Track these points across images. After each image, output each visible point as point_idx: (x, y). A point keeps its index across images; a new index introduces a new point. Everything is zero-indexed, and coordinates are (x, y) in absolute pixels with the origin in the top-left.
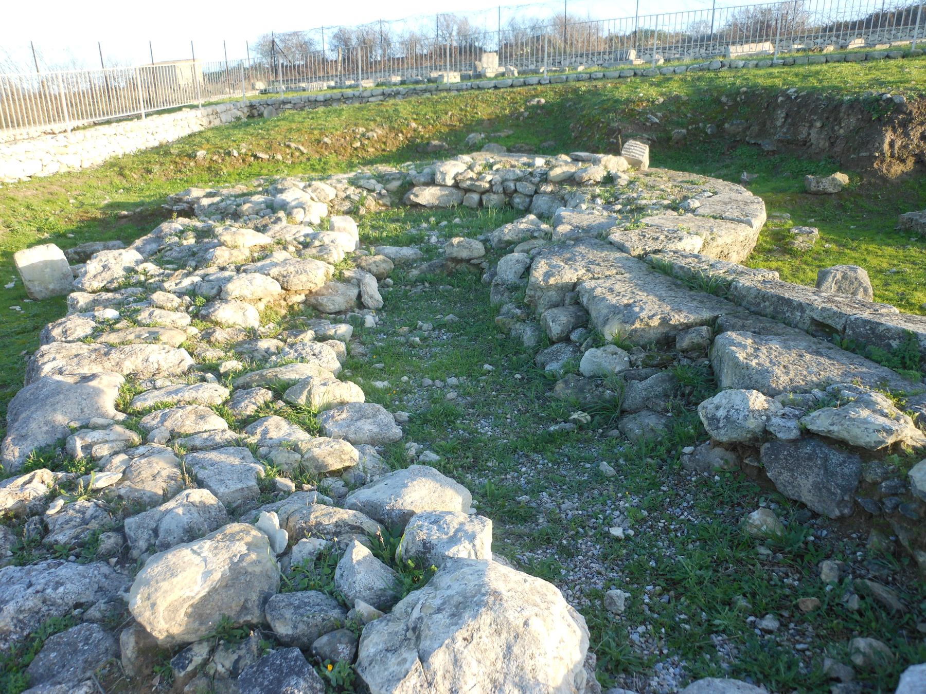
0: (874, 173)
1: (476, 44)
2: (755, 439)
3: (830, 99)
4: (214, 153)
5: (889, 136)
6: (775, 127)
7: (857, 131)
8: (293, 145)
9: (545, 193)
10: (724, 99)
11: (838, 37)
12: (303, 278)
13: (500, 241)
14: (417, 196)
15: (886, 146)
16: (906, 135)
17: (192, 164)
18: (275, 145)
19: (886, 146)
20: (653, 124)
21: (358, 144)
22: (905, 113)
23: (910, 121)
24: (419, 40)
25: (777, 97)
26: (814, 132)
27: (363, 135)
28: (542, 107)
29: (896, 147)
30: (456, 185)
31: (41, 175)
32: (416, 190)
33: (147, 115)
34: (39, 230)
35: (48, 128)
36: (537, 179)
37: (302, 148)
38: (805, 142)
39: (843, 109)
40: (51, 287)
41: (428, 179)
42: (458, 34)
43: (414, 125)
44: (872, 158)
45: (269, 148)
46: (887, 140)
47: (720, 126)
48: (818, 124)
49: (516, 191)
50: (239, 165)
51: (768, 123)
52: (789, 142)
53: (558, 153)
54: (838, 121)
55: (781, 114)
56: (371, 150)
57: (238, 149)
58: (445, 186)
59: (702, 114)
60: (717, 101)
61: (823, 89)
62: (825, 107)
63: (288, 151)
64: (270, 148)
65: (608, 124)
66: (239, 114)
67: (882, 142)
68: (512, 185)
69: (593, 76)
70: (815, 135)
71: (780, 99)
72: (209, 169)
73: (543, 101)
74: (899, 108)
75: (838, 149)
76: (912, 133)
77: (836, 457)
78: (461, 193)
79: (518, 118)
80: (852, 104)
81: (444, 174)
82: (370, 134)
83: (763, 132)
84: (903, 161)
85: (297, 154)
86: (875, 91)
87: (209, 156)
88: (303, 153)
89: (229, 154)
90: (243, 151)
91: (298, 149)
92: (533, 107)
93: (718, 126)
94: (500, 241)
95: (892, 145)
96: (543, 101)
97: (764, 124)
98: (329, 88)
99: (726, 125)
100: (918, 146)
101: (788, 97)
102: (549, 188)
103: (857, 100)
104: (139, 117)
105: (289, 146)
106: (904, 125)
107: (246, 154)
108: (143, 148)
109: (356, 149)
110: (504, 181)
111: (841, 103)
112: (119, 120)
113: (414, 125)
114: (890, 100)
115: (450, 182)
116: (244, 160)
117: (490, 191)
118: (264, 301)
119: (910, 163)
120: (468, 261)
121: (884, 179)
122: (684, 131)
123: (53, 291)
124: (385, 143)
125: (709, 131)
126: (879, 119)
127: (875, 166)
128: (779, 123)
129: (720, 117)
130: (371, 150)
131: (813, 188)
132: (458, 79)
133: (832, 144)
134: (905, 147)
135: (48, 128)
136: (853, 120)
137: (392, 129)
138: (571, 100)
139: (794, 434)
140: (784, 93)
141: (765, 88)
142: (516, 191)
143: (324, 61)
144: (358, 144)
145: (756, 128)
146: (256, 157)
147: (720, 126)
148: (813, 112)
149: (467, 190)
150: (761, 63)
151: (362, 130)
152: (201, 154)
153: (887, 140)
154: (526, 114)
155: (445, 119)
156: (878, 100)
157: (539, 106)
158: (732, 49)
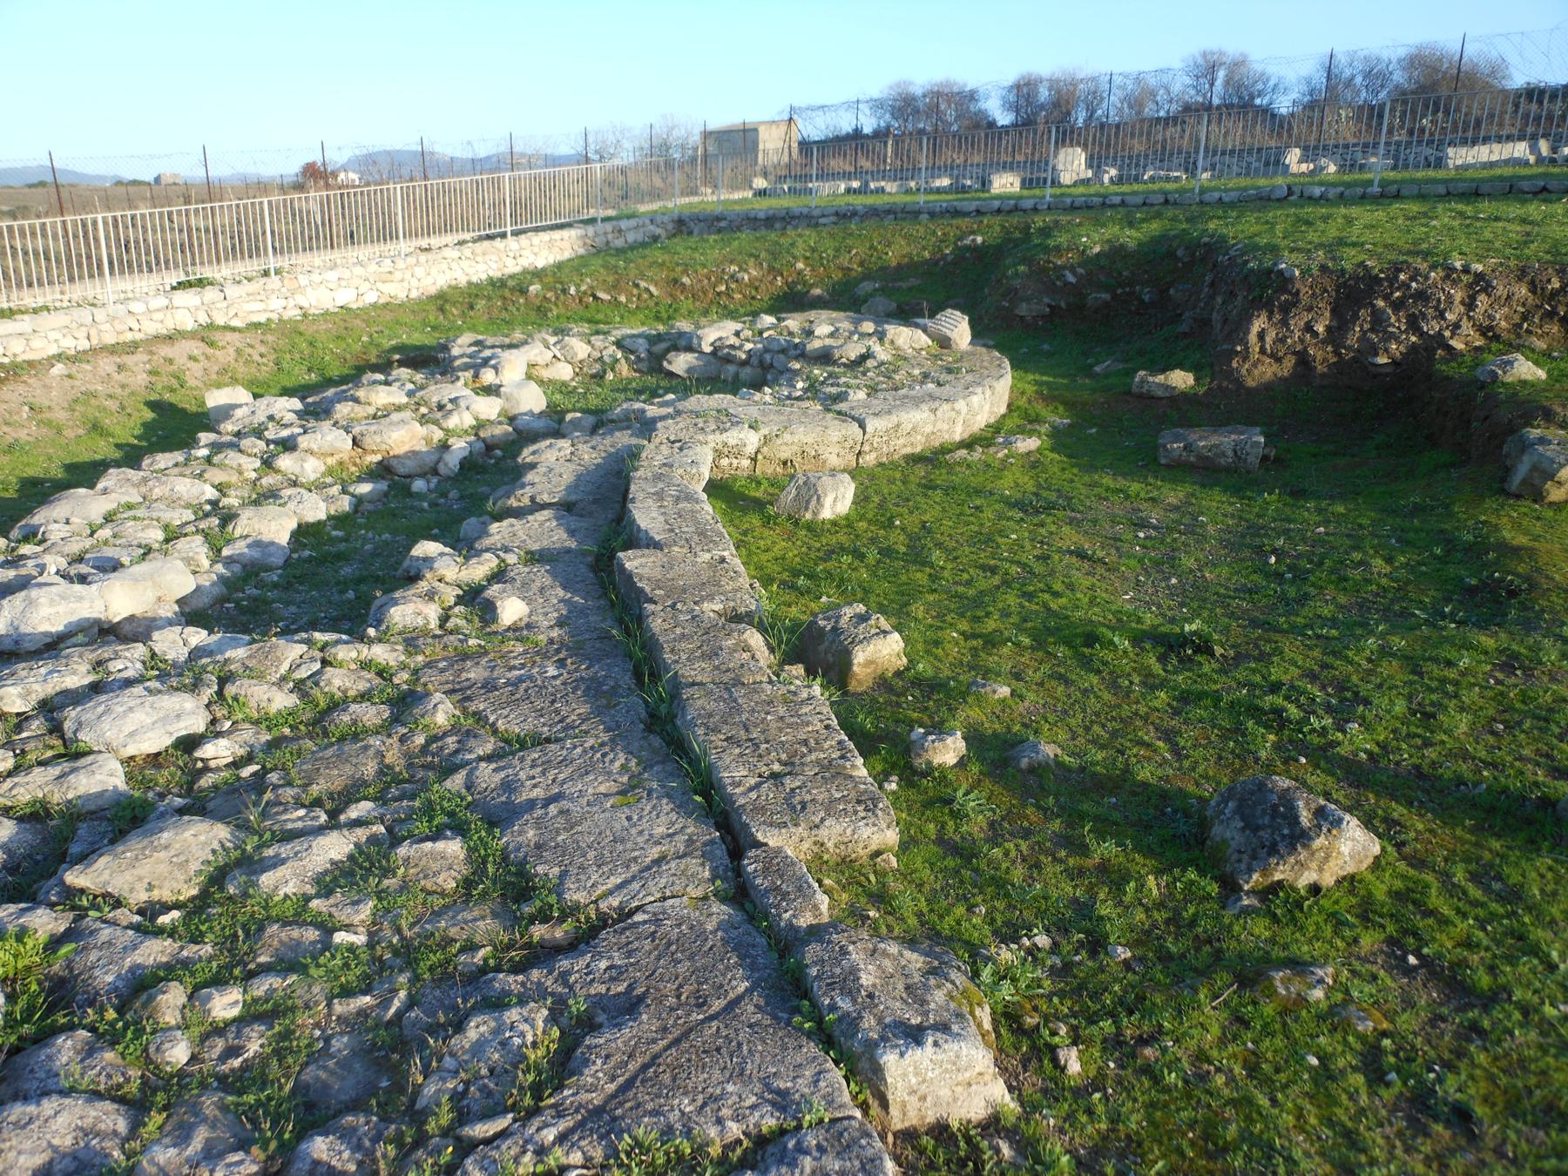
4: (550, 289)
5: (1257, 326)
8: (643, 284)
10: (1180, 253)
12: (378, 439)
16: (1284, 323)
20: (1067, 284)
21: (723, 288)
22: (1290, 293)
23: (1294, 305)
24: (1153, 94)
27: (732, 277)
29: (1268, 340)
31: (354, 306)
33: (516, 233)
34: (310, 370)
35: (424, 243)
37: (652, 289)
42: (1227, 82)
43: (800, 265)
49: (771, 365)
50: (574, 306)
56: (738, 296)
57: (578, 286)
59: (1146, 272)
60: (1171, 255)
63: (635, 291)
64: (614, 287)
66: (658, 231)
67: (1248, 332)
69: (1171, 198)
72: (539, 308)
73: (979, 239)
76: (1292, 322)
84: (1279, 360)
85: (645, 296)
88: (652, 295)
90: (583, 288)
91: (647, 290)
92: (967, 248)
95: (1261, 336)
96: (979, 239)
98: (849, 191)
99: (1172, 291)
100: (1301, 340)
104: (503, 236)
105: (637, 286)
106: (1285, 309)
107: (585, 293)
109: (719, 294)
112: (537, 230)
113: (800, 265)
115: (708, 349)
118: (337, 457)
119: (1289, 362)
121: (1239, 383)
122: (1106, 296)
124: (756, 289)
125: (1146, 298)
127: (1235, 364)
130: (738, 296)
132: (1017, 188)
134: (1282, 340)
135: (424, 243)
137: (771, 269)
143: (992, 124)
144: (723, 288)
146: (595, 297)
150: (1404, 192)
154: (950, 258)
155: (844, 260)
157: (974, 249)
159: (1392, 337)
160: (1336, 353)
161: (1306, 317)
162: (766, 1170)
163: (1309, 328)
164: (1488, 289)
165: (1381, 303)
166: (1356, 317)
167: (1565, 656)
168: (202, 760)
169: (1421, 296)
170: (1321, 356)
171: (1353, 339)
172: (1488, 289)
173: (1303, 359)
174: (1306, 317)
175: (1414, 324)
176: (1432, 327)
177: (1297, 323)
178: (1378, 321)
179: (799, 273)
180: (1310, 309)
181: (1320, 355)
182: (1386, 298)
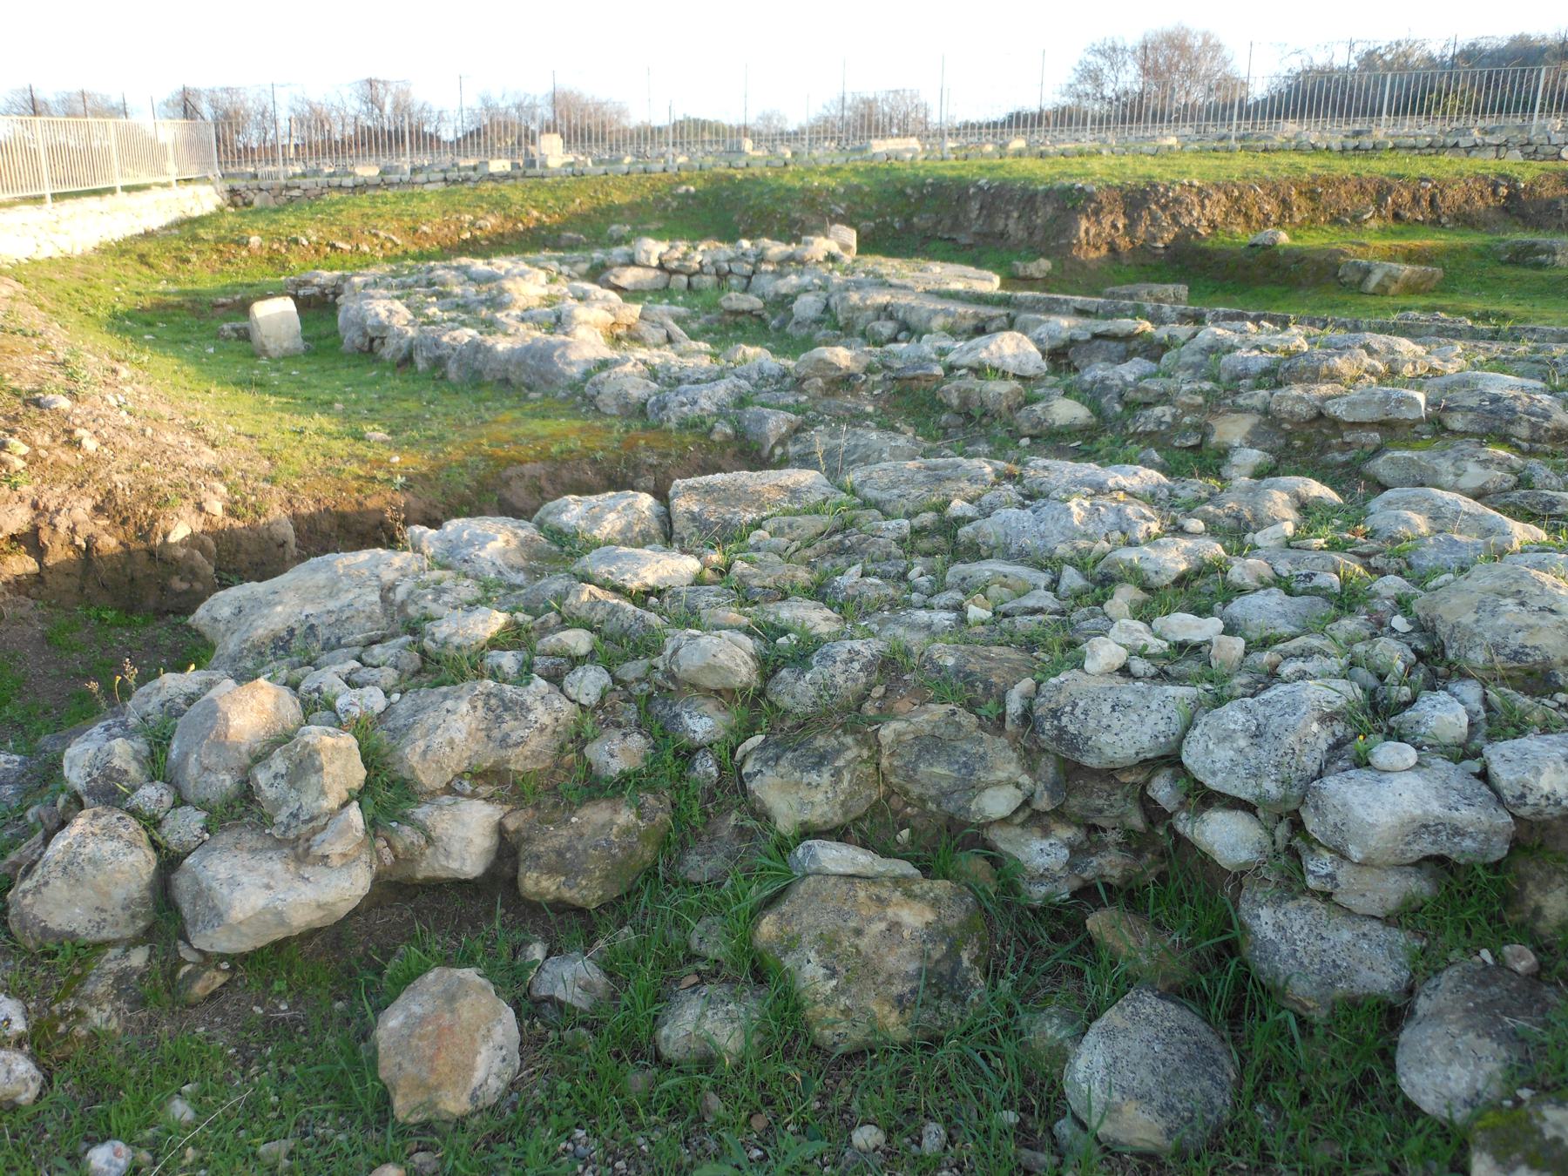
0: (1074, 260)
1: (426, 129)
2: (1065, 346)
3: (1024, 189)
5: (1084, 224)
6: (969, 220)
7: (1055, 219)
8: (382, 234)
9: (766, 272)
10: (909, 191)
11: (994, 136)
13: (777, 294)
14: (617, 277)
15: (1082, 234)
16: (1100, 223)
17: (244, 253)
18: (357, 233)
19: (1082, 234)
25: (967, 188)
26: (1011, 223)
27: (472, 224)
28: (694, 197)
30: (661, 267)
32: (615, 270)
33: (56, 197)
36: (752, 260)
38: (1002, 235)
39: (1039, 198)
40: (285, 345)
41: (626, 259)
43: (535, 213)
44: (1070, 245)
45: (348, 235)
46: (1083, 228)
47: (908, 221)
48: (1015, 215)
49: (730, 272)
51: (961, 217)
52: (986, 235)
53: (759, 236)
54: (1034, 210)
55: (975, 206)
58: (649, 267)
60: (902, 193)
61: (1015, 180)
62: (1025, 198)
65: (788, 215)
67: (1078, 229)
68: (726, 267)
70: (1013, 226)
71: (972, 191)
72: (270, 260)
74: (1090, 197)
75: (1037, 238)
77: (1112, 345)
78: (666, 275)
79: (665, 209)
80: (1048, 193)
81: (648, 253)
82: (481, 223)
83: (956, 225)
84: (1098, 248)
85: (389, 245)
86: (1067, 182)
87: (266, 244)
89: (296, 241)
92: (681, 196)
93: (906, 221)
94: (777, 294)
95: (1087, 232)
96: (692, 189)
97: (956, 218)
99: (915, 220)
101: (980, 188)
102: (770, 268)
103: (1051, 189)
105: (376, 235)
106: (1096, 213)
108: (128, 234)
110: (714, 263)
111: (1036, 193)
113: (535, 213)
114: (1081, 190)
115: (654, 262)
116: (317, 251)
117: (701, 271)
119: (1104, 251)
120: (750, 312)
121: (1083, 265)
123: (286, 350)
125: (897, 226)
126: (1073, 208)
128: (973, 215)
129: (907, 210)
131: (1021, 272)
133: (1031, 234)
134: (1099, 235)
136: (1049, 209)
138: (727, 189)
139: (1088, 336)
140: (975, 184)
141: (952, 179)
142: (730, 272)
145: (948, 222)
146: (333, 246)
147: (908, 221)
148: (1008, 202)
149: (672, 272)
151: (468, 217)
152: (255, 240)
153: (1083, 228)
156: (1070, 189)
158: (874, 142)
159: (1162, 229)
160: (1132, 242)
161: (1111, 218)
162: (1512, 1169)
163: (1114, 226)
164: (1208, 196)
165: (1153, 207)
166: (1140, 217)
167: (1550, 1073)
168: (424, 830)
169: (1176, 200)
170: (1123, 243)
171: (1141, 231)
172: (1208, 196)
173: (1113, 249)
174: (1111, 218)
175: (1175, 219)
176: (1186, 221)
177: (1107, 222)
178: (1154, 219)
179: (538, 220)
180: (1111, 212)
181: (1122, 244)
182: (1157, 203)
